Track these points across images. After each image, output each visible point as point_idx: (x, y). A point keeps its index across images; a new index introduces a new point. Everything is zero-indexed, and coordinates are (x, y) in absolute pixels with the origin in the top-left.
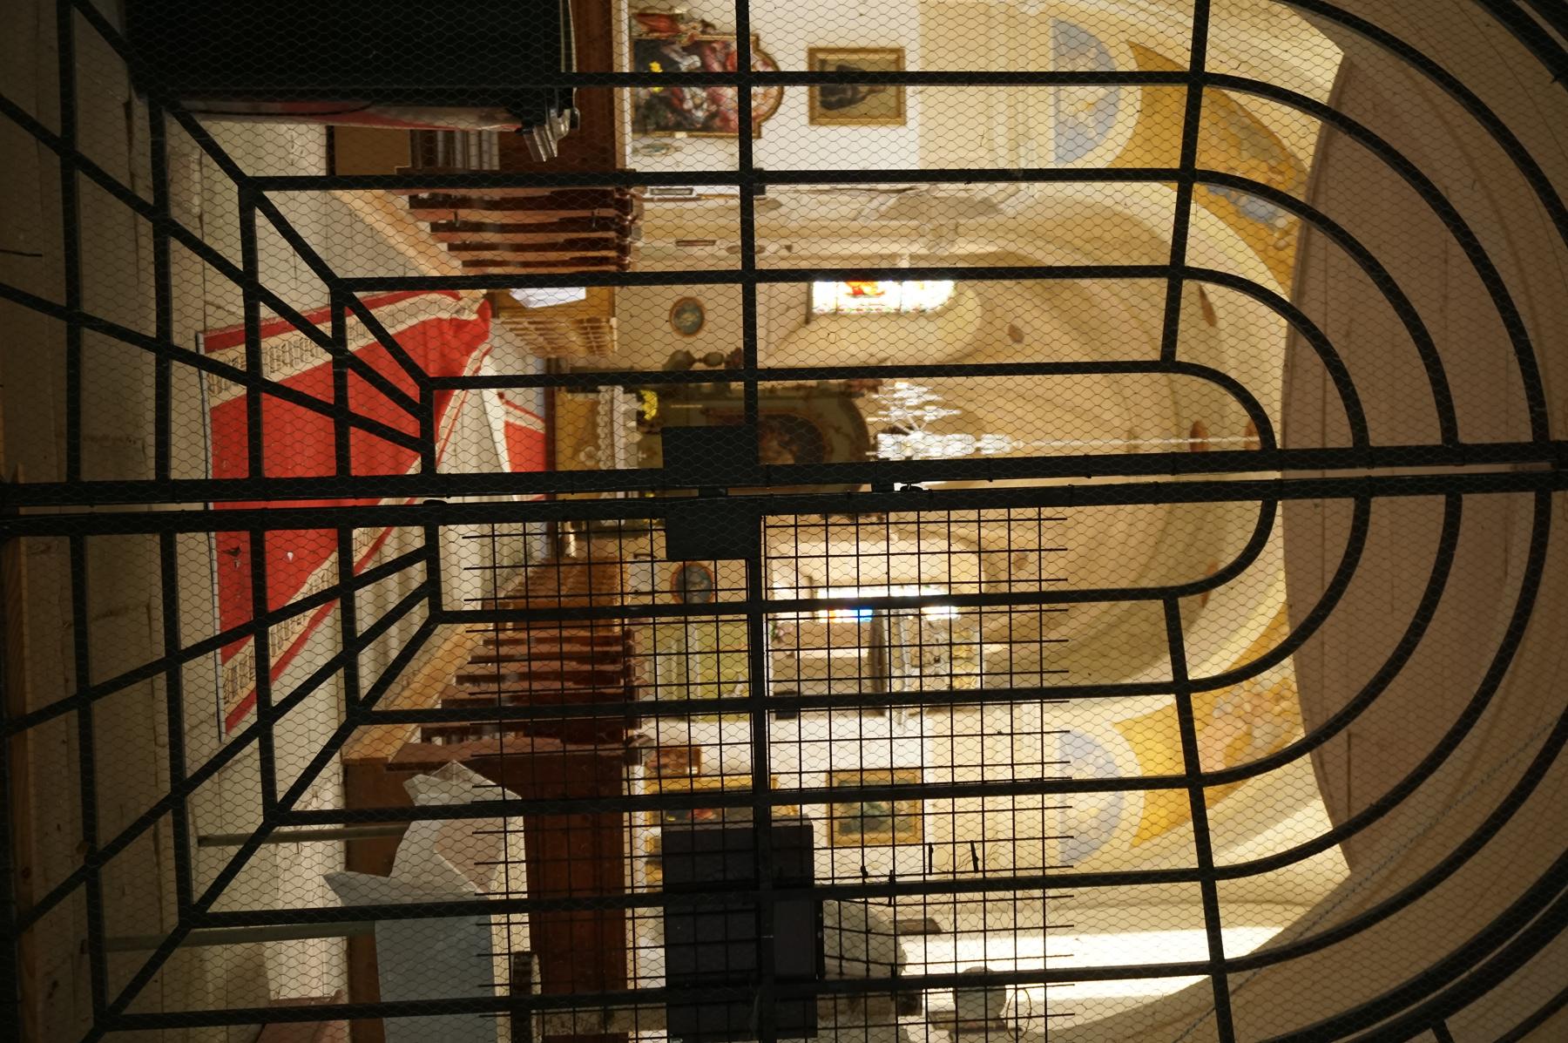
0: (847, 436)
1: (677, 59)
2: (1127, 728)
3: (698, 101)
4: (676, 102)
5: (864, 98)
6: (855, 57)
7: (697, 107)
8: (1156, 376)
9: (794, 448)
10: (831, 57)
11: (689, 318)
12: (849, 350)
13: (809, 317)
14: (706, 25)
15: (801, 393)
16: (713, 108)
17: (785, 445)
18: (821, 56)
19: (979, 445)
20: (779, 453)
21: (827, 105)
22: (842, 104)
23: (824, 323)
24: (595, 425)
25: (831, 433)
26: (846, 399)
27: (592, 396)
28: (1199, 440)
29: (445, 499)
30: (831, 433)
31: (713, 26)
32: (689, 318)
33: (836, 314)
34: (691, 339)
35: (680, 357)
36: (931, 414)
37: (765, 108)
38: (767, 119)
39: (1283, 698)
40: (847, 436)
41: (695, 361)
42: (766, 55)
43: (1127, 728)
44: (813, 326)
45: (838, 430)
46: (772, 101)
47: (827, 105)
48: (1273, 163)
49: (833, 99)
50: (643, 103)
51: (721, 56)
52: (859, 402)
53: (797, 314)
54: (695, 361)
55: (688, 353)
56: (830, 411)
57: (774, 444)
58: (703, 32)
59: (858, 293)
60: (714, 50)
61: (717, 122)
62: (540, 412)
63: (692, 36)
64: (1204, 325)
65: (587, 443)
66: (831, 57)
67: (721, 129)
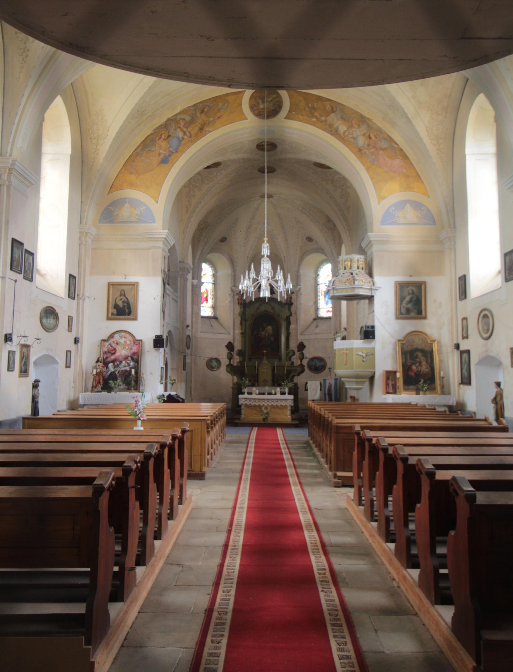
0: (261, 305)
1: (110, 372)
2: (381, 198)
3: (126, 365)
4: (127, 373)
5: (127, 299)
6: (111, 301)
7: (129, 365)
9: (265, 325)
11: (214, 364)
13: (215, 318)
14: (98, 361)
16: (130, 358)
17: (263, 329)
18: (110, 315)
19: (266, 256)
20: (267, 331)
21: (129, 313)
22: (129, 307)
24: (255, 406)
25: (259, 311)
27: (243, 407)
28: (266, 147)
29: (266, 239)
30: (259, 311)
31: (99, 358)
32: (214, 364)
33: (214, 307)
35: (229, 369)
36: (253, 275)
38: (134, 337)
39: (369, 136)
40: (261, 305)
41: (230, 363)
42: (109, 337)
44: (218, 317)
45: (258, 309)
48: (157, 138)
49: (127, 310)
50: (126, 387)
52: (247, 301)
53: (213, 322)
54: (230, 363)
56: (250, 312)
57: (263, 333)
58: (101, 362)
60: (107, 358)
62: (249, 428)
63: (102, 367)
65: (261, 410)
66: (110, 312)
67: (138, 356)
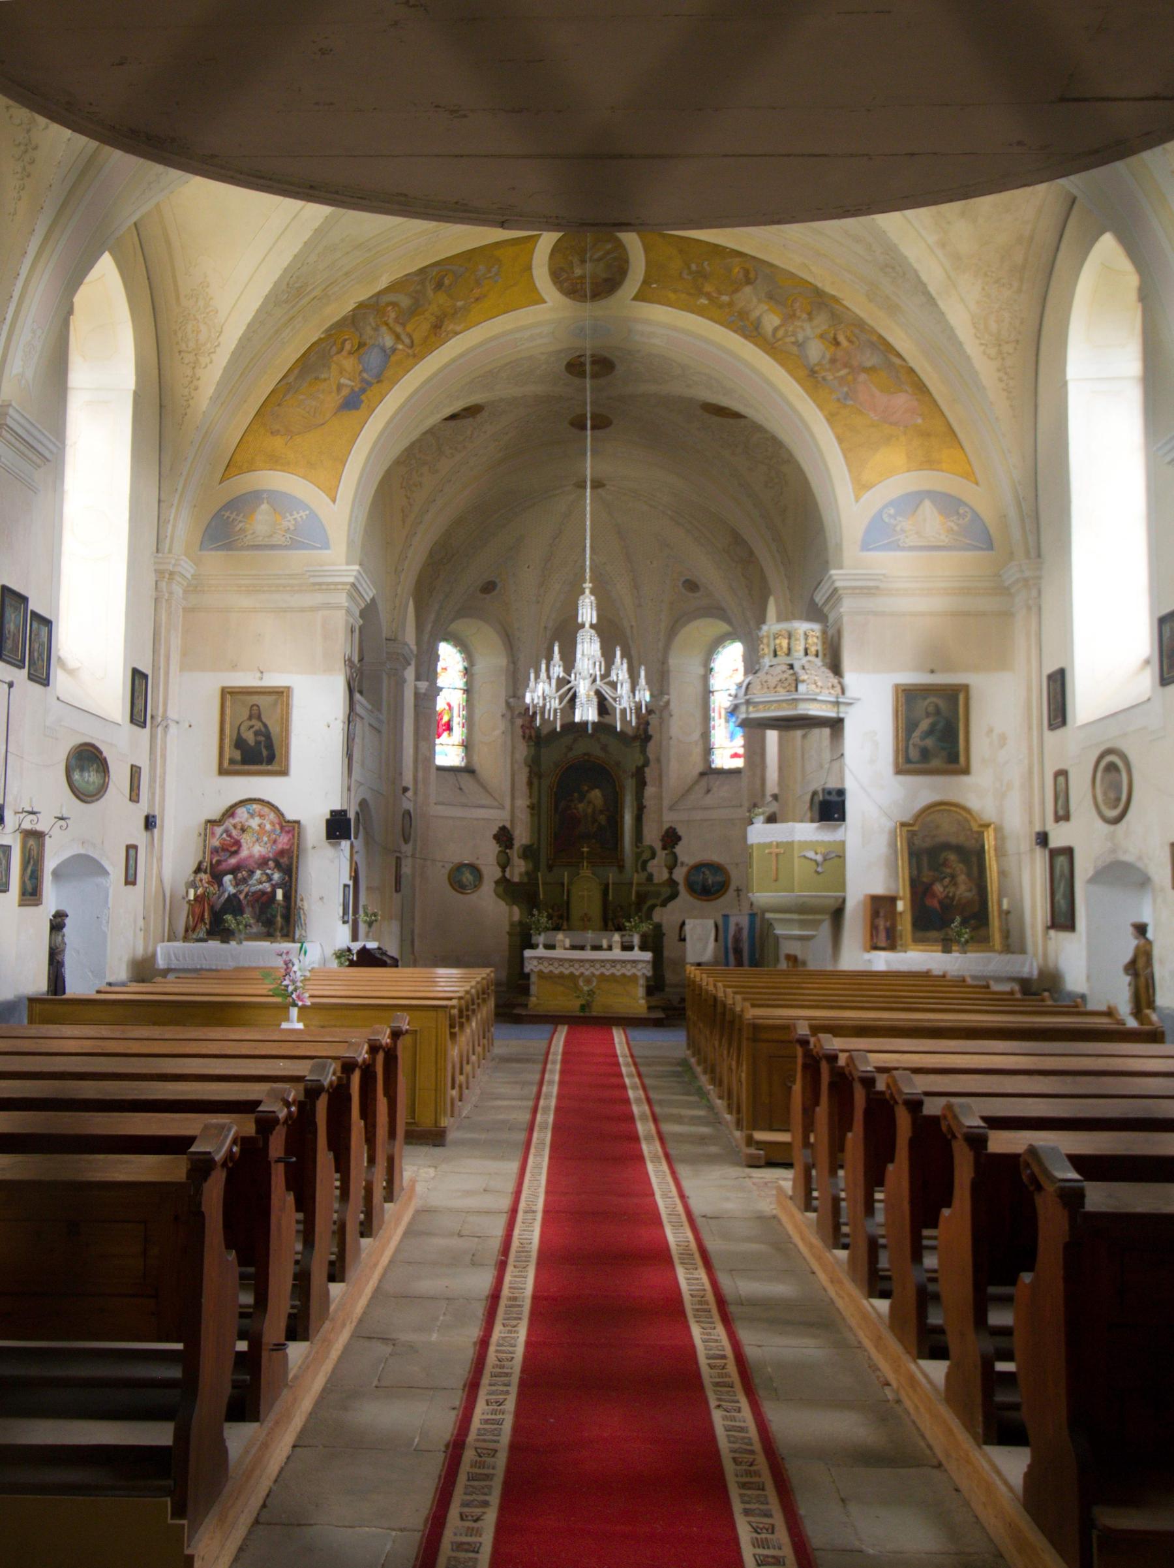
0: (575, 740)
1: (226, 895)
2: (861, 487)
3: (264, 878)
4: (264, 898)
5: (265, 726)
6: (227, 731)
7: (270, 879)
8: (246, 965)
10: (227, 756)
11: (467, 877)
12: (495, 728)
13: (469, 770)
14: (198, 870)
15: (535, 781)
16: (271, 864)
18: (226, 763)
19: (587, 625)
21: (271, 759)
22: (270, 746)
23: (476, 758)
24: (561, 976)
26: (716, 962)
27: (533, 978)
31: (200, 863)
32: (467, 877)
34: (486, 877)
35: (501, 889)
37: (272, 816)
39: (835, 339)
40: (575, 740)
41: (504, 876)
43: (861, 487)
44: (477, 767)
45: (570, 749)
46: (266, 810)
47: (271, 759)
48: (334, 350)
49: (265, 753)
50: (264, 930)
51: (223, 856)
54: (504, 876)
55: (497, 883)
57: (581, 806)
59: (449, 727)
60: (219, 862)
61: (284, 860)
62: (548, 1028)
64: (485, 414)
66: (227, 756)
